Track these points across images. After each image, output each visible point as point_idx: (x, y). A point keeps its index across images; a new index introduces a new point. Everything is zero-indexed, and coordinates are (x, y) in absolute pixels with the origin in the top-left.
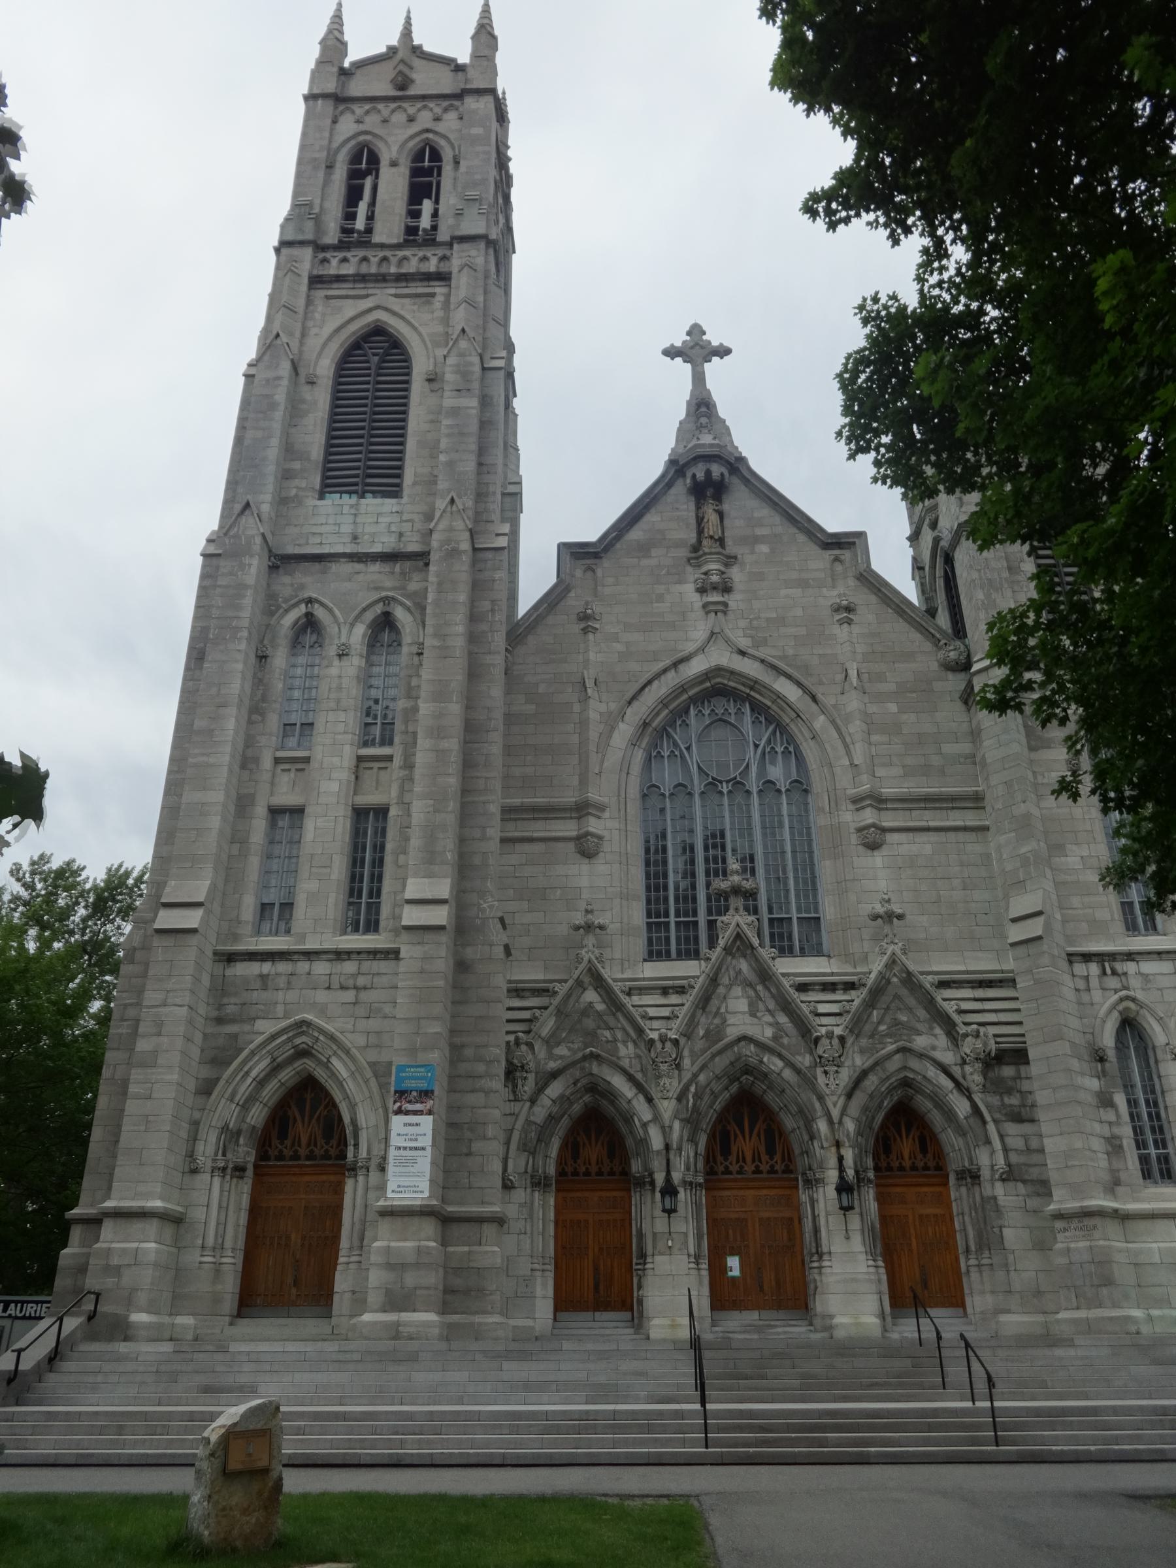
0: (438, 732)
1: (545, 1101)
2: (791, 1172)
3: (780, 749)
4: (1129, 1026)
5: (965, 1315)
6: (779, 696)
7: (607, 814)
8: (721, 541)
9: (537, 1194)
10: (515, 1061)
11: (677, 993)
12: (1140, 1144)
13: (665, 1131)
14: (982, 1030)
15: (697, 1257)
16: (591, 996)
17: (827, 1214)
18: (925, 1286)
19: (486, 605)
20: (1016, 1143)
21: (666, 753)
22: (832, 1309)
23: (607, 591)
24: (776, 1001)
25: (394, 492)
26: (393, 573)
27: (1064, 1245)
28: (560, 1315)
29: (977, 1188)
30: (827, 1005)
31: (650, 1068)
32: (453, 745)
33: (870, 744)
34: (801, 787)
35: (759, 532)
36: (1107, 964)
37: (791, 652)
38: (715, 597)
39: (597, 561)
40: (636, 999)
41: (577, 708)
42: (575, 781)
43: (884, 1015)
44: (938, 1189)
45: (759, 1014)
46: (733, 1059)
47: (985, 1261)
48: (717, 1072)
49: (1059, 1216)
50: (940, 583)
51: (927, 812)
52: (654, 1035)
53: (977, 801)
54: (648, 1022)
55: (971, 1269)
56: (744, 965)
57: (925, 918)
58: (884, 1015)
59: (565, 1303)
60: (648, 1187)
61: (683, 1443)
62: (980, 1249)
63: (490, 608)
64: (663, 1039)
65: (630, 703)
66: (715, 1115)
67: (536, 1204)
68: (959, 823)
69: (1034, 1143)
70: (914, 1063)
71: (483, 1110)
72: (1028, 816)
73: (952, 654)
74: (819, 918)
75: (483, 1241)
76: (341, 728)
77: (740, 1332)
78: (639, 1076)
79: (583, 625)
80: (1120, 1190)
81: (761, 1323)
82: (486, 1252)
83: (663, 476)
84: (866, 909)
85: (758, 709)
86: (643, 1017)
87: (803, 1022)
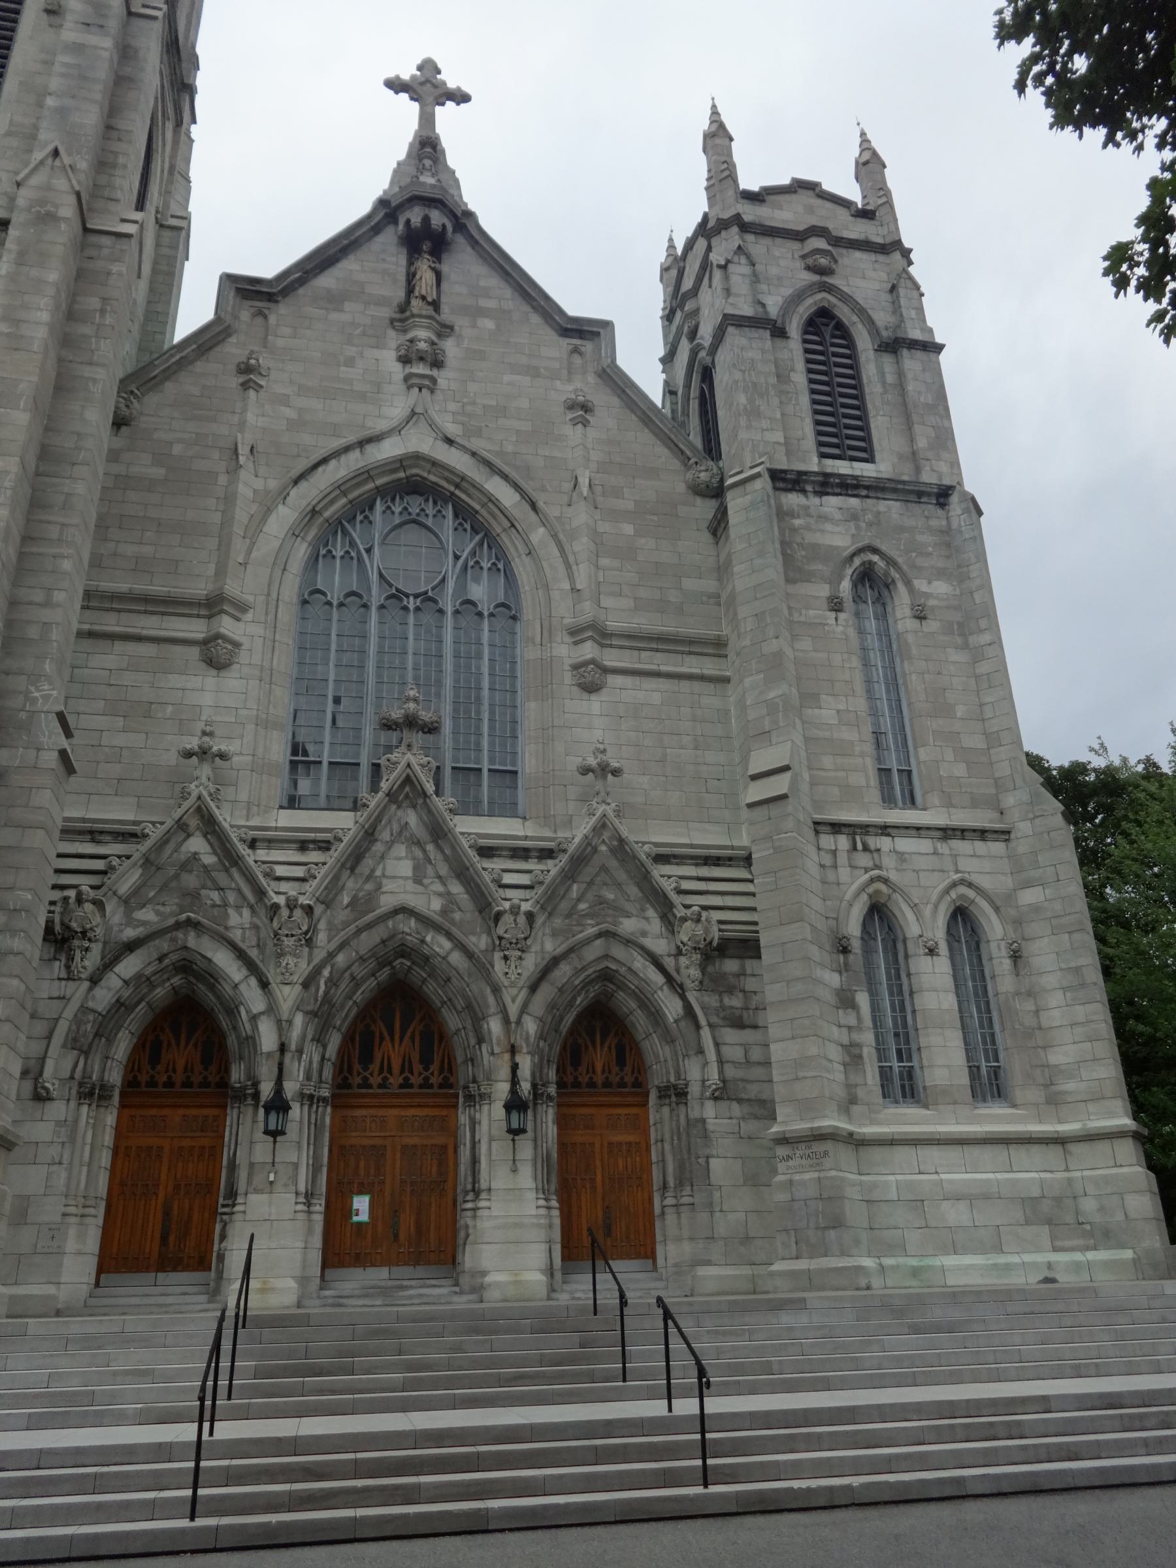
2: (451, 1086)
3: (486, 565)
4: (879, 913)
5: (655, 1268)
6: (491, 499)
7: (249, 616)
8: (436, 305)
9: (85, 1109)
10: (74, 925)
11: (320, 849)
13: (282, 1026)
14: (704, 914)
16: (197, 844)
18: (608, 1232)
19: (94, 303)
20: (734, 1053)
21: (339, 553)
23: (280, 343)
24: (451, 867)
29: (682, 1108)
31: (270, 943)
33: (597, 567)
34: (508, 611)
35: (483, 303)
36: (858, 838)
37: (510, 448)
38: (420, 369)
40: (262, 854)
41: (223, 479)
42: (211, 570)
43: (586, 891)
44: (634, 1110)
45: (426, 881)
46: (385, 937)
47: (685, 1200)
48: (362, 952)
49: (783, 1140)
50: (694, 405)
51: (658, 654)
52: (281, 900)
54: (273, 884)
55: (668, 1210)
56: (412, 818)
58: (586, 891)
59: (116, 1259)
60: (250, 1101)
61: (151, 1510)
62: (680, 1184)
63: (98, 306)
64: (292, 905)
65: (296, 482)
69: (756, 1054)
70: (618, 951)
72: (779, 654)
73: (702, 475)
74: (516, 772)
77: (359, 1297)
78: (253, 953)
79: (242, 379)
80: (855, 1109)
81: (390, 1283)
83: (369, 217)
84: (575, 762)
85: (463, 513)
86: (266, 875)
87: (482, 893)
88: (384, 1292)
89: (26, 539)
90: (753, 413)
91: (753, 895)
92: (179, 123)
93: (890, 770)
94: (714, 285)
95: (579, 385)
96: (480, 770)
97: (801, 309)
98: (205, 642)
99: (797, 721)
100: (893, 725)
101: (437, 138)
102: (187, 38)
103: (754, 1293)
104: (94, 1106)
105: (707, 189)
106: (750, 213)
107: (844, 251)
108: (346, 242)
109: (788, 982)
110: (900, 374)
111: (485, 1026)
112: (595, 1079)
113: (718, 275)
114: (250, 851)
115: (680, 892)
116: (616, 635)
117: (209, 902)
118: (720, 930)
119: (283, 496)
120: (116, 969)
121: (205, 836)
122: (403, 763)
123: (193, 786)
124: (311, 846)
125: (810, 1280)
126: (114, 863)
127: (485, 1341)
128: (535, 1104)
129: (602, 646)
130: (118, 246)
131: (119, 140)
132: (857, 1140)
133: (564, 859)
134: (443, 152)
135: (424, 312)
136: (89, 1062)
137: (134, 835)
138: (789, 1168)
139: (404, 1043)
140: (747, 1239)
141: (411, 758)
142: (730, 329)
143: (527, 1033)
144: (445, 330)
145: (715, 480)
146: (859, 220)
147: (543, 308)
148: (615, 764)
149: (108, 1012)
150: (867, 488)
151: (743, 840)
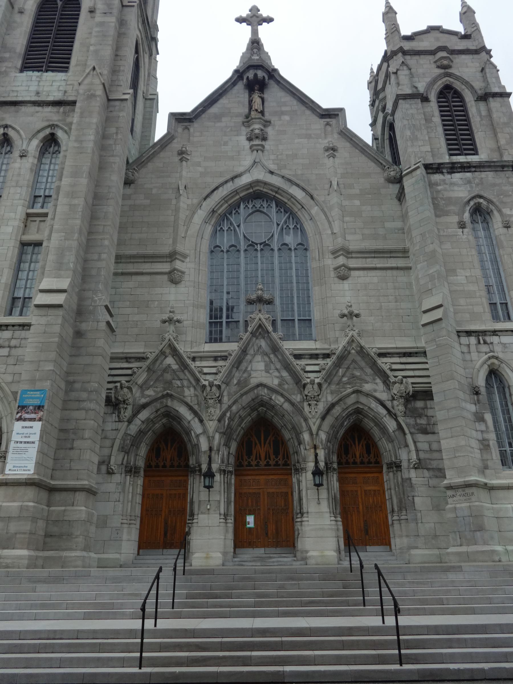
0: (72, 195)
1: (137, 422)
2: (288, 465)
3: (292, 227)
4: (494, 374)
6: (292, 196)
7: (188, 260)
8: (262, 113)
9: (128, 477)
10: (120, 398)
11: (223, 360)
12: (500, 444)
13: (210, 439)
14: (404, 380)
15: (226, 516)
16: (170, 361)
17: (307, 489)
22: (307, 547)
23: (195, 139)
25: (66, 69)
26: (58, 112)
27: (453, 506)
28: (141, 551)
29: (399, 473)
30: (312, 367)
31: (203, 402)
32: (80, 202)
33: (343, 222)
34: (303, 247)
35: (284, 109)
36: (481, 338)
37: (299, 172)
38: (257, 142)
39: (191, 124)
40: (198, 363)
41: (174, 202)
42: (171, 241)
43: (346, 372)
44: (376, 475)
45: (271, 371)
46: (254, 397)
47: (403, 517)
48: (244, 405)
49: (450, 487)
50: (387, 142)
51: (375, 259)
52: (206, 383)
53: (404, 253)
54: (203, 376)
55: (395, 522)
56: (263, 343)
57: (372, 318)
59: (147, 543)
60: (197, 473)
61: (123, 662)
62: (400, 510)
63: (115, 132)
64: (211, 385)
65: (205, 199)
66: (242, 431)
67: (128, 483)
68: (394, 265)
69: (435, 446)
70: (363, 399)
71: (83, 421)
72: (434, 251)
74: (311, 320)
75: (75, 503)
76: (17, 196)
78: (196, 407)
80: (487, 472)
81: (265, 555)
82: (76, 510)
83: (230, 79)
84: (337, 312)
85: (280, 204)
86: (200, 372)
88: (261, 559)
89: (90, 233)
90: (414, 139)
91: (428, 369)
92: (151, 55)
93: (496, 304)
94: (391, 83)
95: (330, 140)
96: (294, 320)
97: (436, 87)
98: (170, 273)
99: (446, 283)
100: (496, 282)
101: (259, 39)
102: (152, 17)
103: (441, 562)
104: (132, 476)
105: (385, 38)
106: (407, 46)
107: (456, 56)
108: (221, 91)
109: (448, 410)
110: (489, 110)
111: (302, 437)
112: (356, 461)
113: (393, 77)
114: (193, 363)
115: (392, 370)
116: (354, 252)
117: (176, 386)
118: (413, 387)
119: (200, 205)
120: (138, 416)
121: (173, 357)
122: (257, 318)
123: (166, 335)
124: (219, 359)
125: (468, 557)
126: (135, 370)
127: (295, 584)
128: (327, 472)
129: (348, 258)
130: (122, 105)
131: (121, 60)
132: (490, 487)
133: (334, 357)
134: (262, 45)
135: (257, 117)
136: (129, 457)
137: (143, 358)
138: (454, 501)
139: (266, 446)
140: (435, 536)
141: (261, 316)
142: (400, 101)
143: (322, 439)
144: (267, 123)
145: (398, 175)
146: (463, 40)
147: (311, 107)
148: (356, 312)
149: (136, 435)
150: (475, 167)
151: (422, 344)
